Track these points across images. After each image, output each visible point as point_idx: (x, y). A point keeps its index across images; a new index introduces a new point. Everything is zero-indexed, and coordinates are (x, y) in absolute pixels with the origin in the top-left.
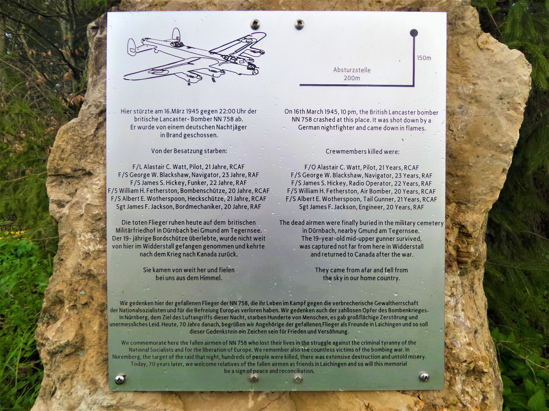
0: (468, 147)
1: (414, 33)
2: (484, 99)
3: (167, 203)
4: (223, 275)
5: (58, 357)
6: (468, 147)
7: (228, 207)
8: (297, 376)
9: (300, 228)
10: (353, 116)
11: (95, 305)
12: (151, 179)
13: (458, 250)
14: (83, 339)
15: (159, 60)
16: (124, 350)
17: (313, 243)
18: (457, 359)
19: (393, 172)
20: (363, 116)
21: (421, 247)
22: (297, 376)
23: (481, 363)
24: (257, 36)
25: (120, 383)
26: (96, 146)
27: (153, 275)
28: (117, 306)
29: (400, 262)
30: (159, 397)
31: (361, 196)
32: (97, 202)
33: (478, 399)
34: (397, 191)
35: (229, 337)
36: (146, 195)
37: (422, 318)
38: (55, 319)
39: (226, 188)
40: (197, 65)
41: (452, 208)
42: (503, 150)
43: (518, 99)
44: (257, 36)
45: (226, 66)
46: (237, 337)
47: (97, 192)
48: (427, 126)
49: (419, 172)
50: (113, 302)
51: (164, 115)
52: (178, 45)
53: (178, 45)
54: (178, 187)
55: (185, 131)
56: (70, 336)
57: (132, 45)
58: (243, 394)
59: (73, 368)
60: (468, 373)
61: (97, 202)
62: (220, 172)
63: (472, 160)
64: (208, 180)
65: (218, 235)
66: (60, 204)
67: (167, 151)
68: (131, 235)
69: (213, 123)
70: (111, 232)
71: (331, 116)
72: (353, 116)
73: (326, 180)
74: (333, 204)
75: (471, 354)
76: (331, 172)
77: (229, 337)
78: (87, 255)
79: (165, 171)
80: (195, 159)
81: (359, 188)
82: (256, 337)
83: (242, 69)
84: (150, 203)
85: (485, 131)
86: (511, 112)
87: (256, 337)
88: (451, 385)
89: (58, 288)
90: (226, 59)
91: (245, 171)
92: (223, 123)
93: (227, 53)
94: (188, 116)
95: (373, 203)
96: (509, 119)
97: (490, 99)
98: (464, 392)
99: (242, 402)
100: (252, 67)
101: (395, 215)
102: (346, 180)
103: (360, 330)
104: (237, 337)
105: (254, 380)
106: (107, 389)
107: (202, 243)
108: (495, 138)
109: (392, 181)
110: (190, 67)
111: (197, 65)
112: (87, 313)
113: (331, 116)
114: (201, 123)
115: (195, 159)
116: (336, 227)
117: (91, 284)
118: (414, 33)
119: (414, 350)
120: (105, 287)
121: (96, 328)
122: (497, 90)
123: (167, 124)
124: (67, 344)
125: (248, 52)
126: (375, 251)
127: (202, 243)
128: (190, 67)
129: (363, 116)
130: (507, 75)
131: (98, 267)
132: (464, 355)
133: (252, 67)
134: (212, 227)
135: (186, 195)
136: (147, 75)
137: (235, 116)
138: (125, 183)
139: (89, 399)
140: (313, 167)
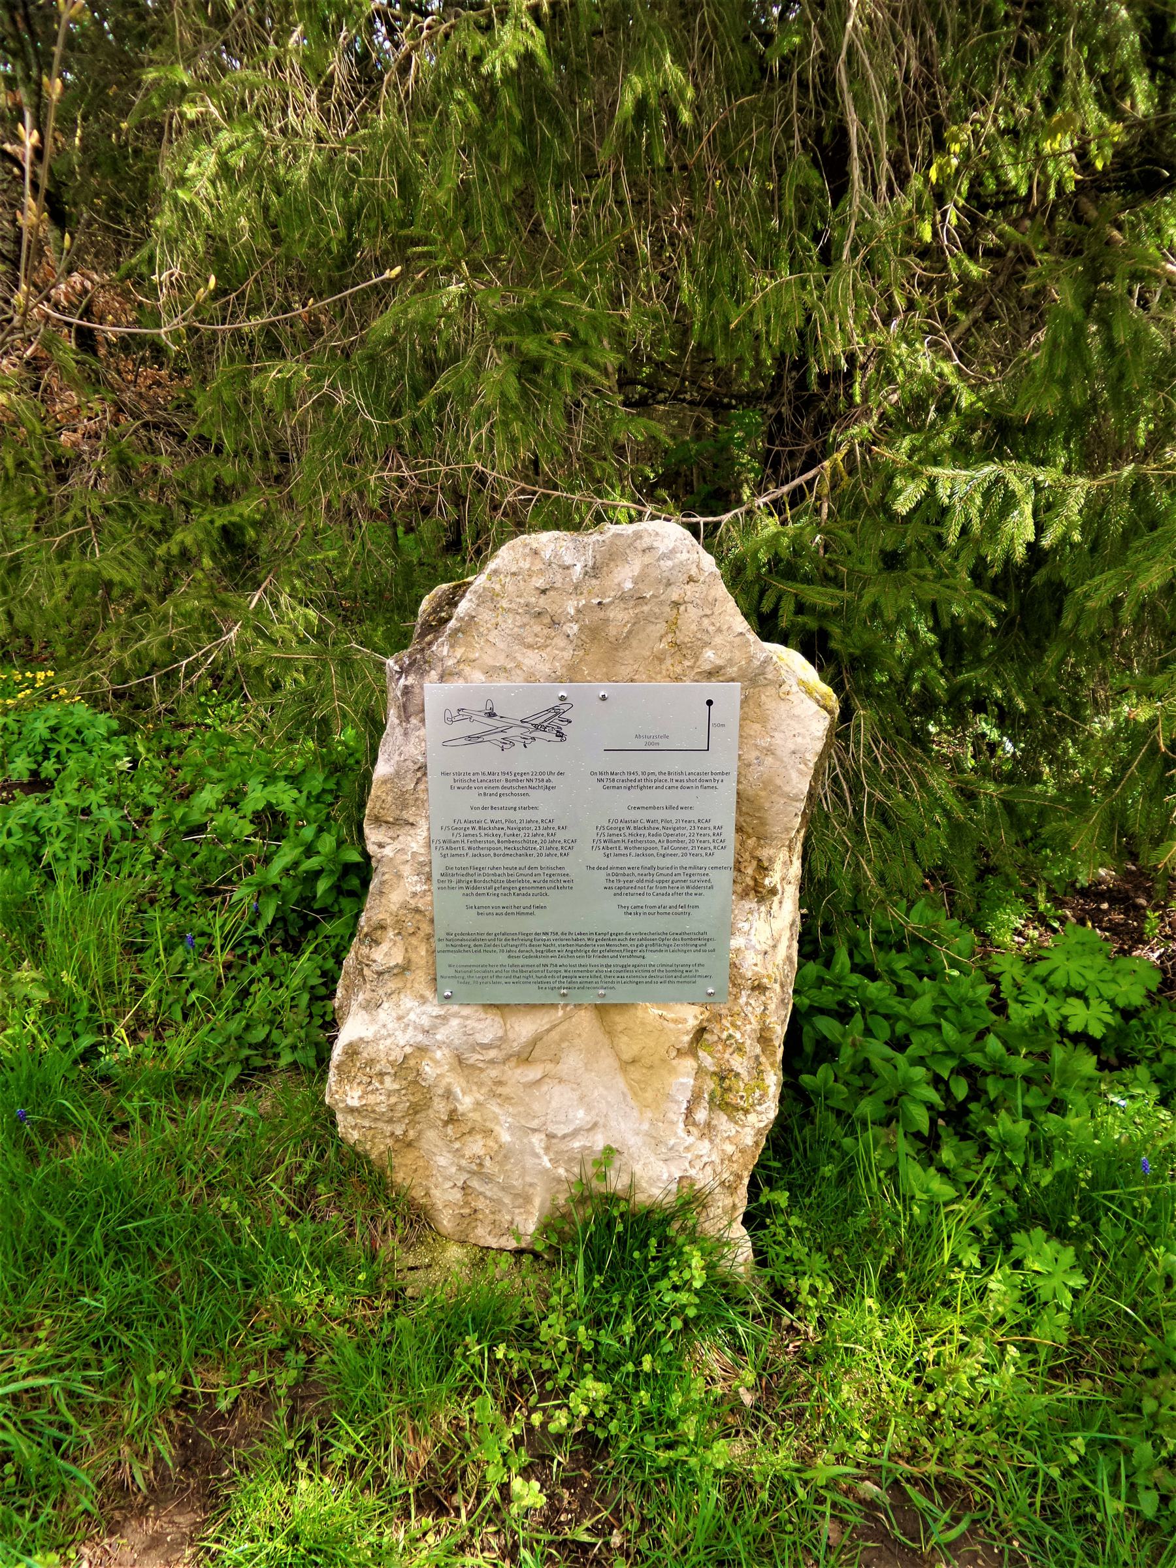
0: (763, 794)
1: (710, 703)
2: (778, 752)
3: (485, 852)
4: (536, 911)
5: (386, 976)
6: (763, 794)
7: (540, 855)
8: (601, 992)
9: (604, 872)
10: (653, 777)
11: (421, 934)
12: (470, 832)
13: (755, 880)
14: (409, 961)
15: (475, 729)
16: (451, 972)
17: (616, 884)
18: (742, 977)
19: (688, 825)
20: (662, 777)
21: (711, 888)
22: (601, 992)
23: (765, 980)
24: (565, 707)
25: (447, 997)
26: (417, 799)
27: (475, 911)
28: (443, 936)
29: (693, 900)
30: (481, 1010)
31: (659, 845)
32: (422, 851)
33: (759, 1011)
34: (692, 841)
35: (543, 961)
36: (466, 846)
37: (710, 945)
38: (377, 943)
39: (538, 839)
40: (510, 733)
41: (21, 1509)
42: (796, 799)
43: (809, 756)
44: (565, 707)
45: (536, 734)
46: (548, 961)
47: (422, 842)
48: (720, 785)
49: (711, 825)
50: (440, 933)
51: (481, 777)
52: (491, 715)
53: (491, 715)
54: (495, 839)
55: (500, 791)
56: (398, 958)
57: (448, 715)
58: (554, 1006)
59: (400, 985)
60: (753, 989)
61: (422, 851)
62: (533, 826)
63: (767, 805)
64: (522, 833)
65: (531, 879)
66: (381, 846)
67: (484, 808)
68: (454, 879)
69: (526, 784)
70: (436, 876)
71: (632, 777)
72: (653, 777)
73: (627, 832)
74: (634, 852)
75: (756, 973)
76: (632, 825)
77: (543, 961)
78: (415, 894)
79: (483, 825)
80: (511, 815)
81: (656, 839)
82: (566, 961)
83: (553, 737)
84: (471, 852)
85: (778, 782)
86: (802, 766)
87: (566, 961)
88: (736, 998)
89: (381, 916)
90: (536, 727)
91: (555, 825)
92: (534, 784)
93: (537, 722)
94: (503, 778)
95: (669, 852)
96: (800, 772)
97: (784, 753)
98: (748, 1004)
99: (553, 1011)
100: (560, 735)
101: (688, 861)
102: (646, 832)
103: (655, 956)
104: (548, 961)
105: (564, 995)
106: (436, 1002)
107: (518, 885)
108: (787, 789)
109: (687, 832)
110: (504, 735)
111: (510, 733)
112: (414, 941)
113: (632, 777)
114: (515, 784)
115: (511, 815)
116: (636, 872)
117: (417, 917)
118: (710, 703)
119: (702, 971)
120: (432, 921)
121: (423, 953)
122: (791, 746)
123: (484, 784)
124: (397, 966)
125: (556, 721)
126: (671, 891)
127: (518, 885)
128: (504, 735)
129: (662, 777)
130: (802, 731)
131: (426, 904)
132: (749, 974)
133: (560, 735)
134: (527, 871)
135: (502, 846)
136: (463, 741)
137: (546, 777)
138: (448, 835)
139: (418, 1011)
140: (616, 821)
